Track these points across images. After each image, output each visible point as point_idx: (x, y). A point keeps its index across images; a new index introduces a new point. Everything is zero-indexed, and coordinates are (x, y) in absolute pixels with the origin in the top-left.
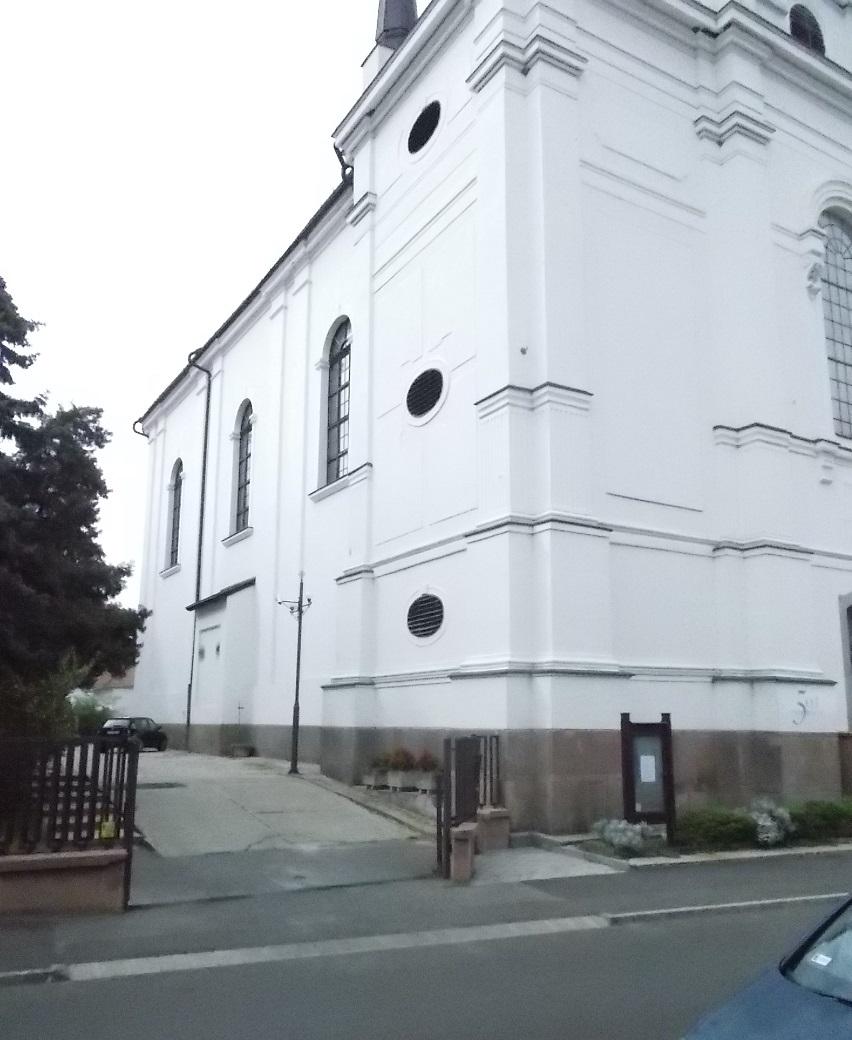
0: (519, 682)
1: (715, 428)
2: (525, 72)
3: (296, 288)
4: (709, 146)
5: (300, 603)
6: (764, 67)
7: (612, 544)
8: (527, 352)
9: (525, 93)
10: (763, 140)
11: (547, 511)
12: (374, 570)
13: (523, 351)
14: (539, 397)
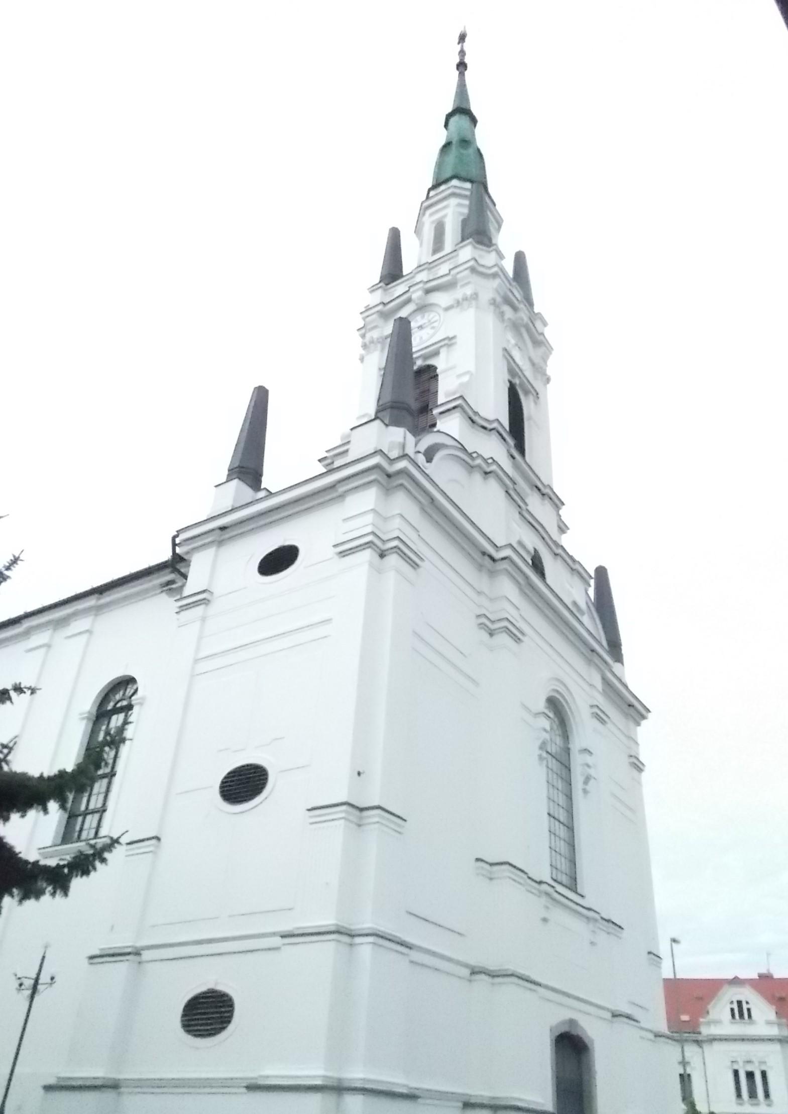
0: (329, 1099)
1: (478, 860)
2: (382, 555)
3: (69, 634)
4: (484, 635)
5: (37, 980)
6: (423, 510)
7: (412, 962)
8: (362, 775)
9: (379, 571)
10: (518, 640)
11: (367, 924)
12: (142, 952)
13: (359, 774)
14: (369, 817)
